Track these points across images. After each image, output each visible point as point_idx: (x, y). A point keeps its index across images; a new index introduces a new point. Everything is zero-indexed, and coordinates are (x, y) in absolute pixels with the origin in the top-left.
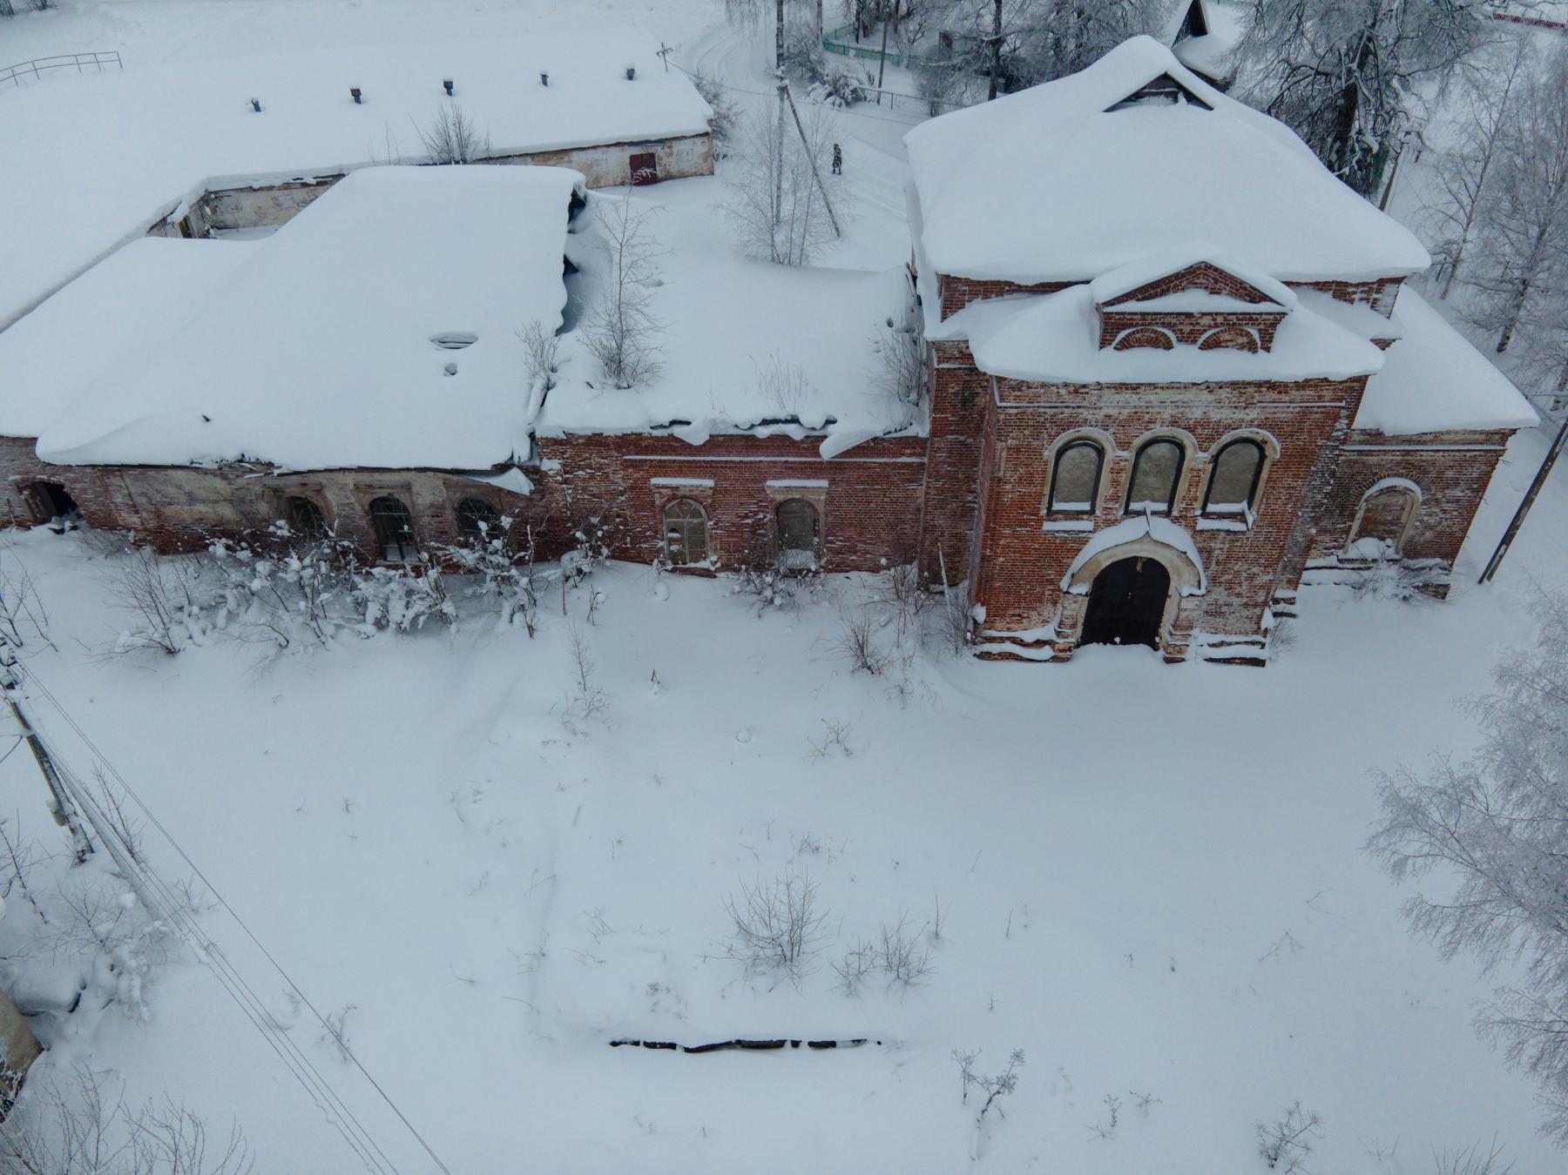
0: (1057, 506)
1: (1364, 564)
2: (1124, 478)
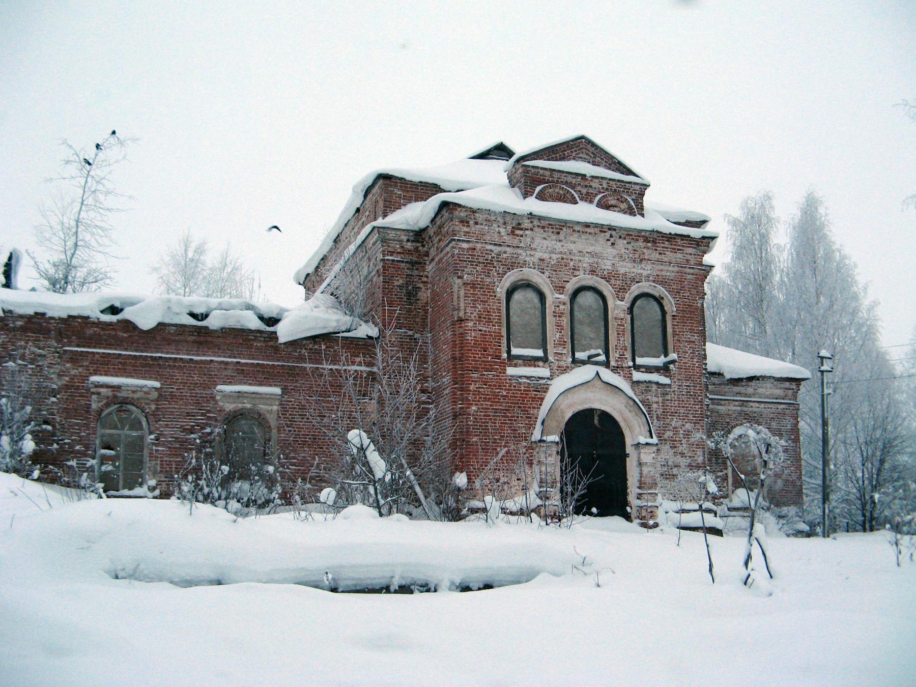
0: (515, 351)
2: (566, 321)
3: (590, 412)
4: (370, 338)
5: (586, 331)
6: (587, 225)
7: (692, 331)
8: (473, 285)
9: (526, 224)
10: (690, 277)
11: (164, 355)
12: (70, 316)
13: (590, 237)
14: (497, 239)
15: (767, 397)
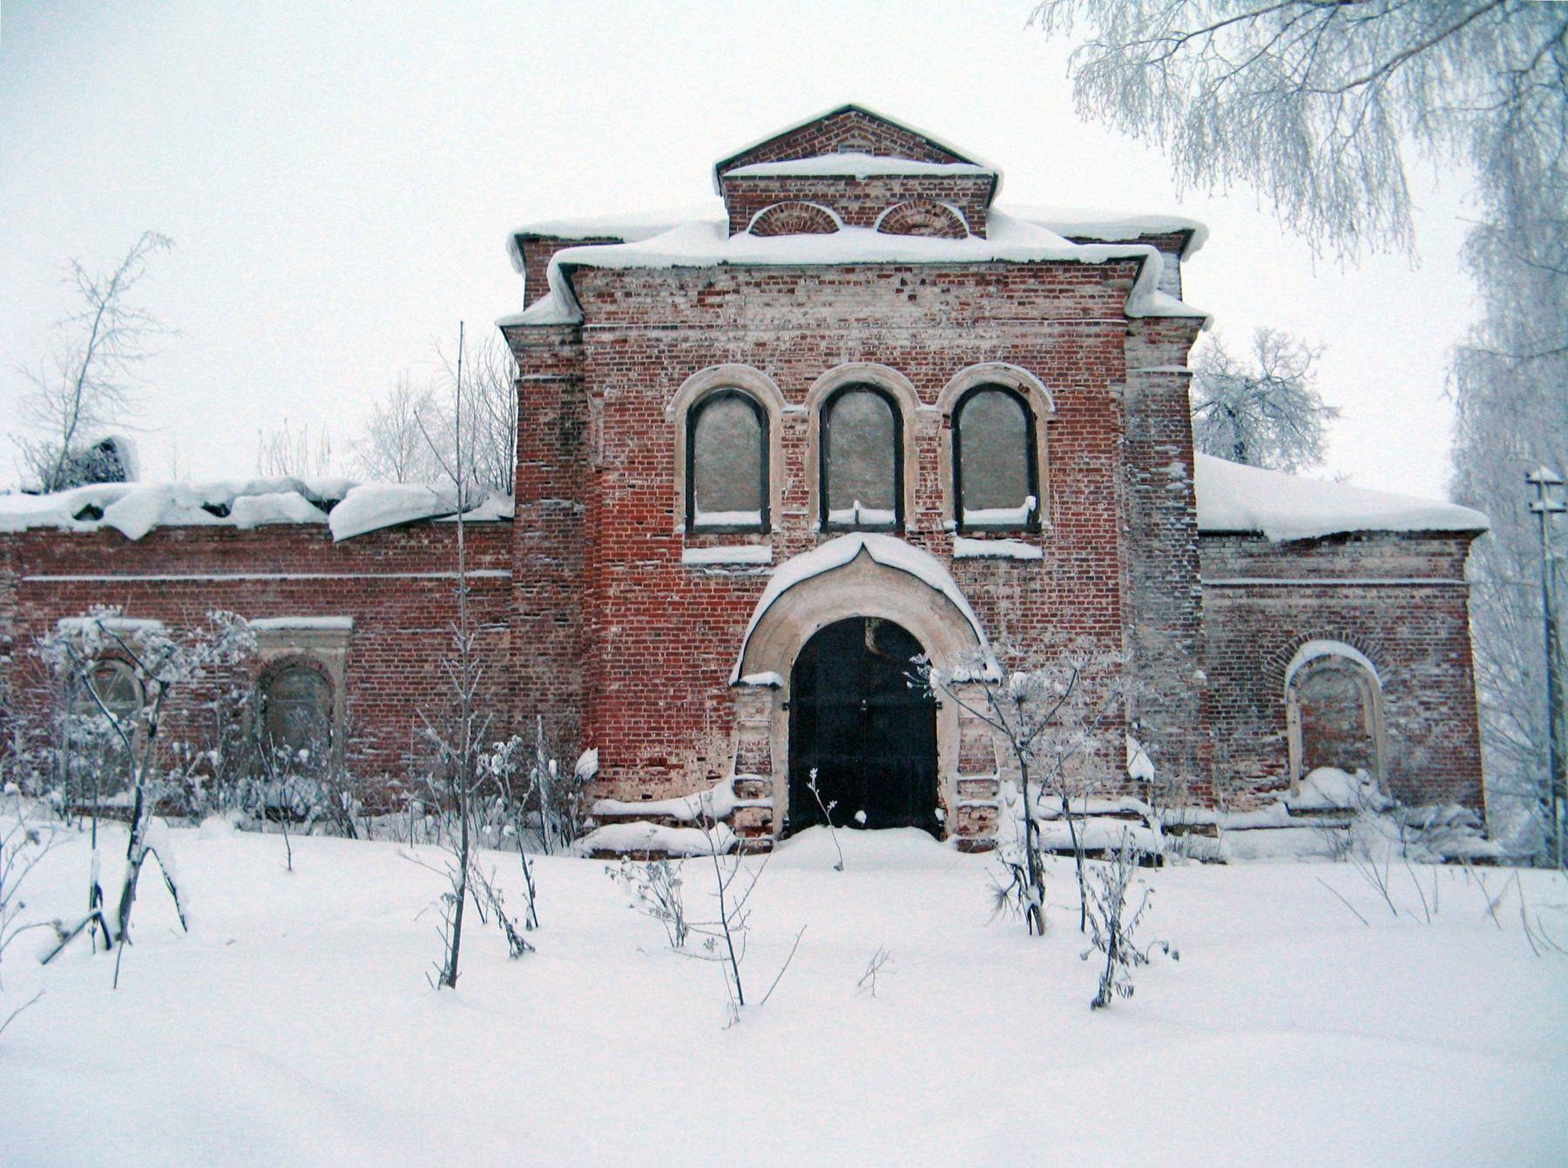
0: (702, 519)
1: (1339, 813)
2: (809, 454)
3: (856, 625)
4: (504, 519)
5: (853, 468)
6: (849, 269)
7: (1092, 448)
8: (622, 407)
9: (723, 282)
10: (1091, 341)
11: (169, 578)
12: (30, 529)
13: (859, 289)
14: (670, 319)
15: (1387, 574)
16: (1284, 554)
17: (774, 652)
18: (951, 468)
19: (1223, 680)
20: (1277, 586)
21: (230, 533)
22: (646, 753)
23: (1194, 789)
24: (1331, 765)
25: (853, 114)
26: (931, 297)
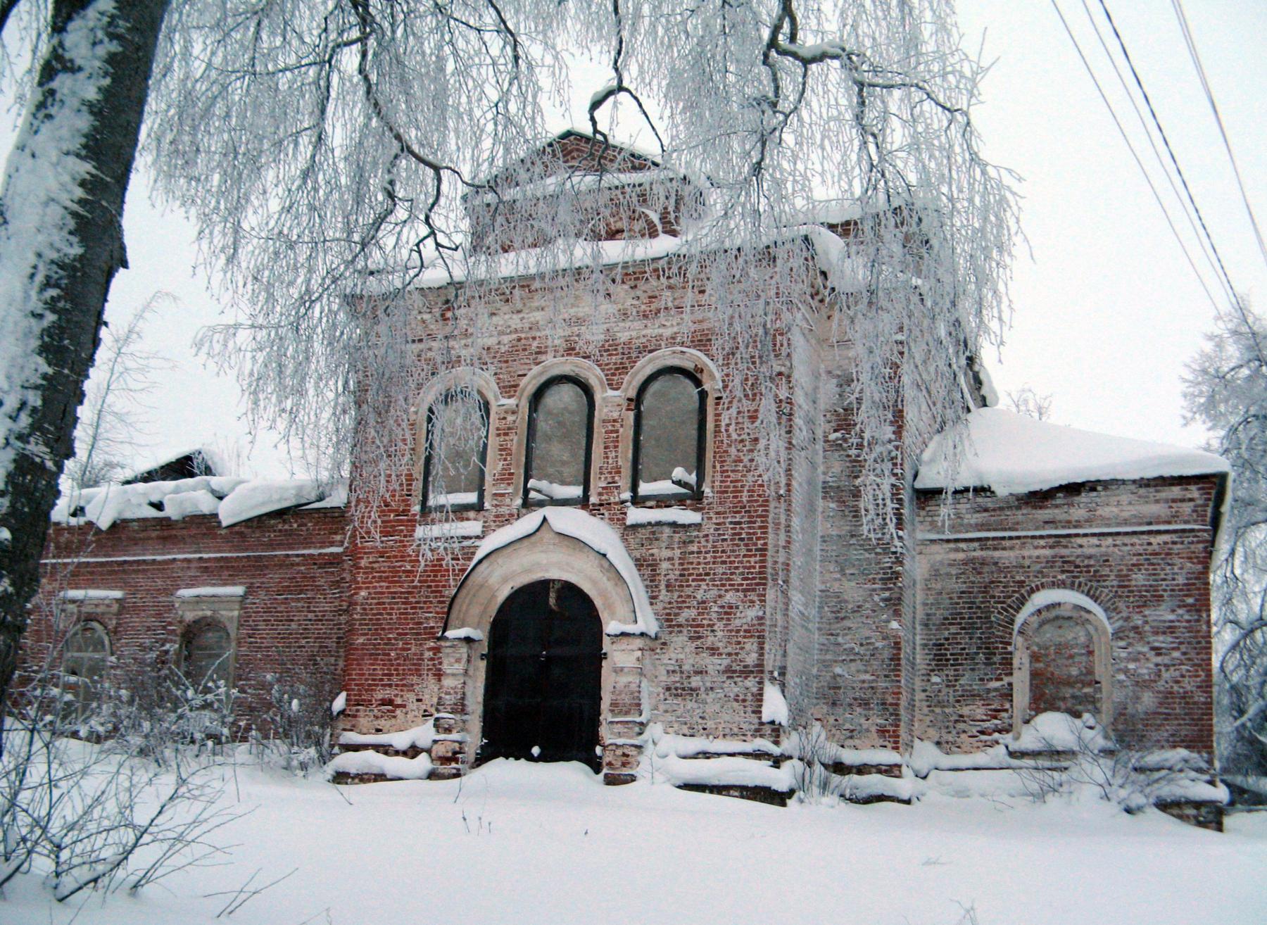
1: (1054, 755)
2: (517, 442)
3: (543, 586)
5: (557, 451)
14: (420, 332)
15: (1126, 522)
16: (1018, 508)
17: (475, 611)
18: (631, 447)
19: (953, 629)
20: (1011, 538)
21: (166, 523)
22: (380, 694)
23: (882, 732)
24: (1058, 709)
25: (572, 138)
26: (622, 294)
